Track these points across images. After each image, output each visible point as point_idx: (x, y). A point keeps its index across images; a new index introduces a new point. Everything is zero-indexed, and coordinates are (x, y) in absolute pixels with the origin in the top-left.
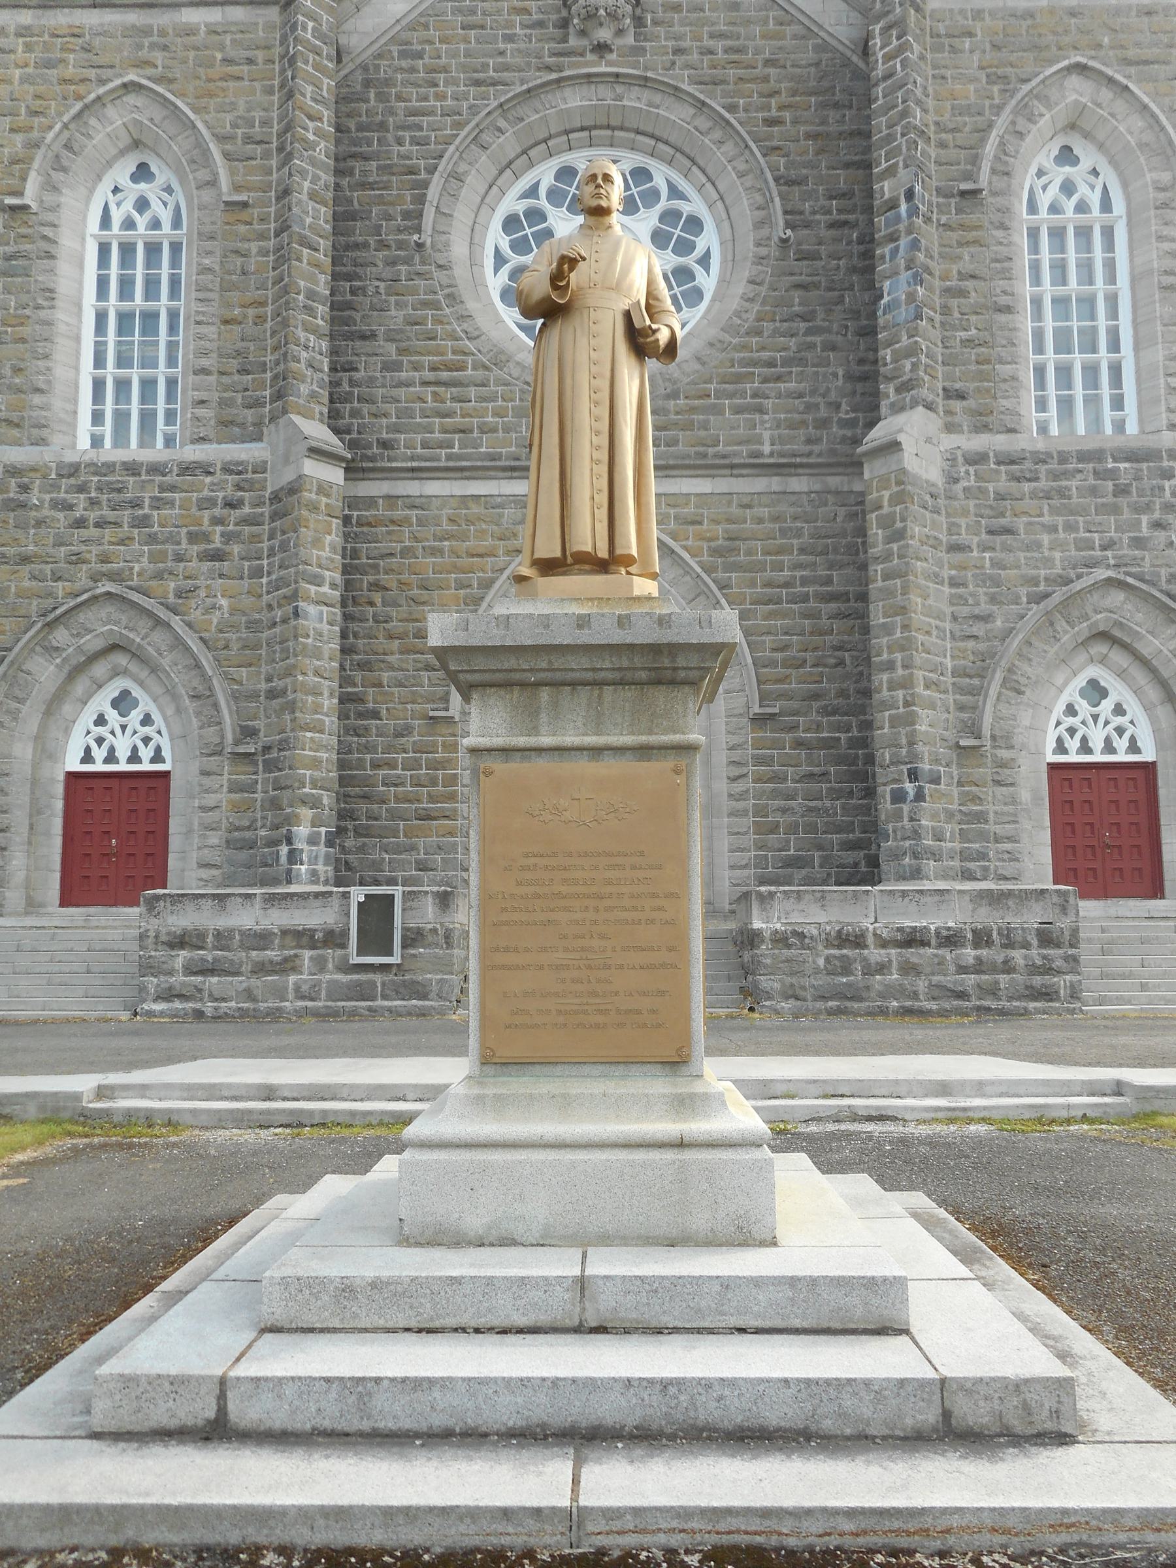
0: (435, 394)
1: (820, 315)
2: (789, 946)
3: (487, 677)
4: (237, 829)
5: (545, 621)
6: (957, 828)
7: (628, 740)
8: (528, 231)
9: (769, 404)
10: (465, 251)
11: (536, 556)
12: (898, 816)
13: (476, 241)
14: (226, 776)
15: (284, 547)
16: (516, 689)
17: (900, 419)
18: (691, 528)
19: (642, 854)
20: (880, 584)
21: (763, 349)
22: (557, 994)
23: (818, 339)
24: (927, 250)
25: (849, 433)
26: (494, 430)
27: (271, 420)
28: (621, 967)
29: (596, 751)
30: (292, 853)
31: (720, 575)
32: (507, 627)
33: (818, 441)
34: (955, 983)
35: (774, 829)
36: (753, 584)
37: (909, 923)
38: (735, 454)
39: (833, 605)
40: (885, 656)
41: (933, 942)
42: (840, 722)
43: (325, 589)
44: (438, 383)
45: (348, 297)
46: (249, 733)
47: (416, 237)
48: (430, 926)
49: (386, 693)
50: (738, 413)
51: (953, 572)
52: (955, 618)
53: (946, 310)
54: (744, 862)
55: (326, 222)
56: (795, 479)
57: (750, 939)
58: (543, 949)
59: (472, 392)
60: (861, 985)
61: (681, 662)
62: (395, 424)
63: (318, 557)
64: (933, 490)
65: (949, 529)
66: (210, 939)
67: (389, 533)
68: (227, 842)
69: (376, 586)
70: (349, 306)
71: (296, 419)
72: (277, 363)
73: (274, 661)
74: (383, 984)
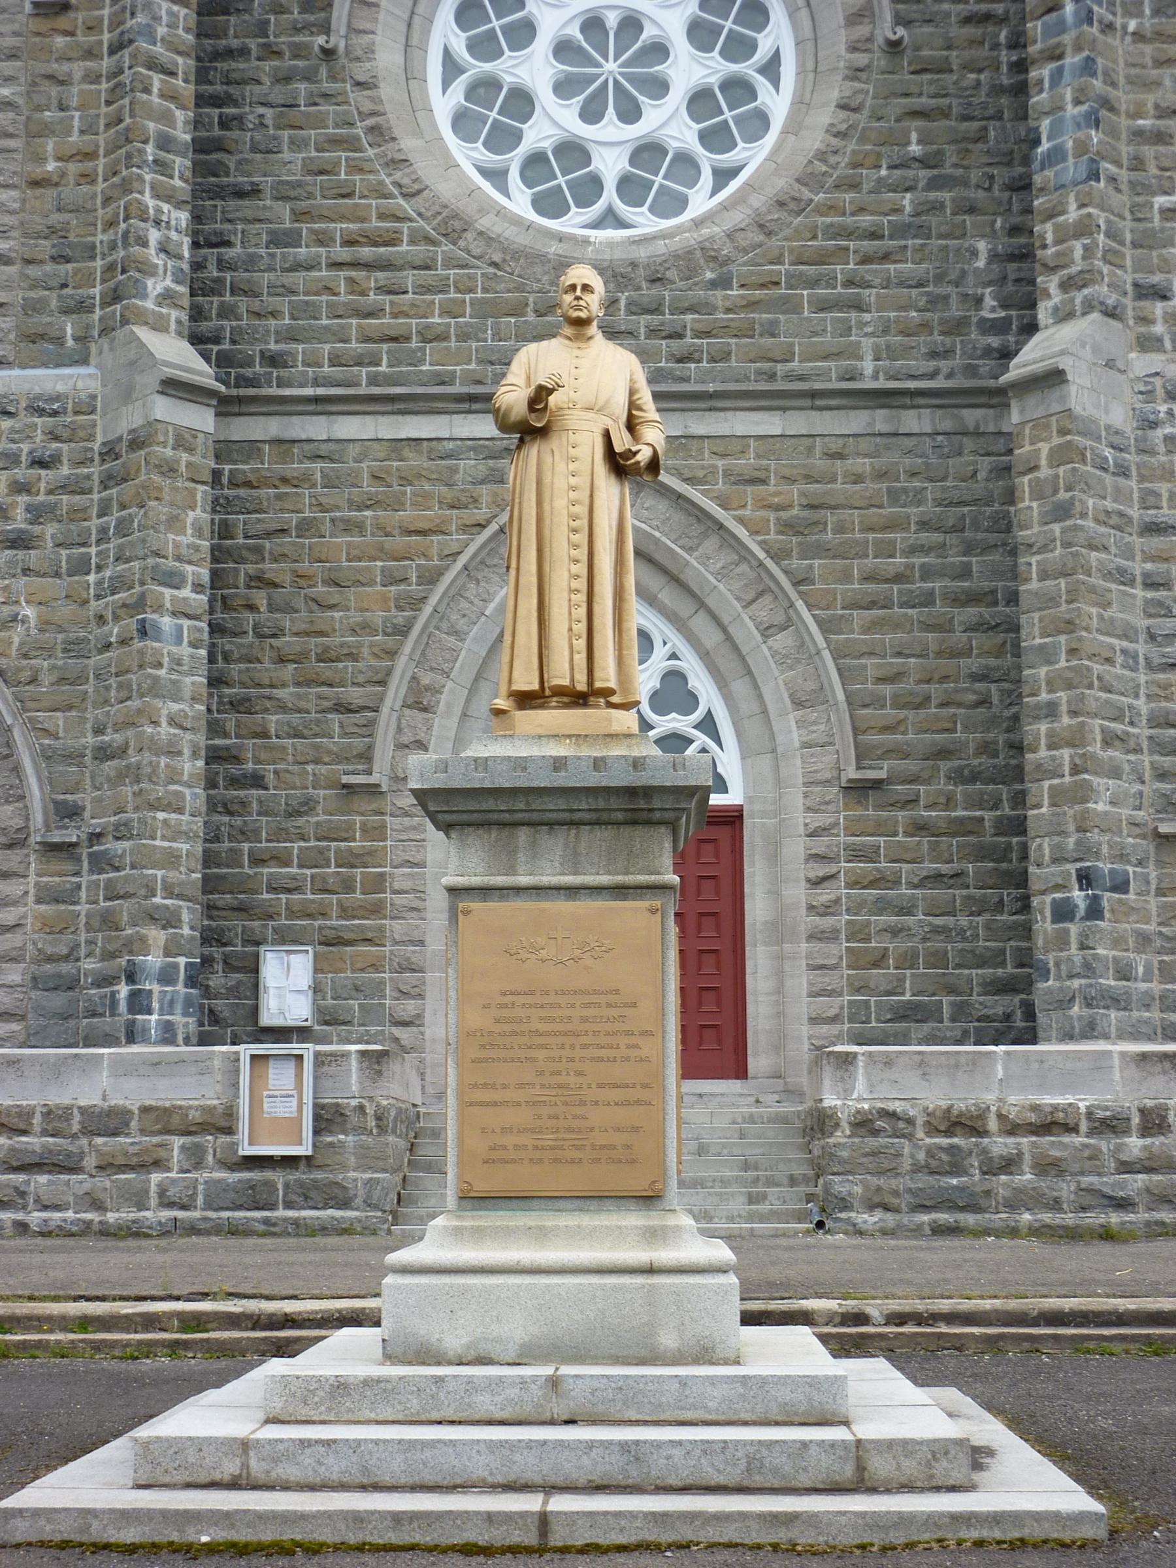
0: (351, 281)
1: (951, 158)
2: (876, 1133)
3: (465, 817)
4: (50, 959)
5: (521, 764)
6: (1156, 960)
7: (604, 879)
8: (496, 24)
9: (870, 295)
10: (399, 59)
11: (514, 688)
12: (1062, 941)
13: (414, 41)
14: (32, 879)
15: (123, 528)
16: (494, 829)
17: (1068, 332)
18: (749, 489)
19: (617, 992)
20: (1034, 585)
21: (862, 210)
22: (533, 1131)
23: (946, 196)
24: (1106, 74)
25: (994, 341)
26: (443, 337)
27: (104, 332)
28: (597, 1103)
29: (572, 891)
30: (134, 995)
31: (795, 563)
32: (486, 770)
33: (947, 353)
34: (1113, 1185)
35: (879, 961)
36: (847, 577)
37: (1049, 1100)
38: (822, 375)
39: (972, 611)
40: (1044, 696)
41: (1084, 1126)
42: (982, 793)
43: (186, 592)
44: (355, 265)
45: (217, 132)
46: (68, 812)
47: (321, 40)
48: (354, 1102)
49: (272, 748)
50: (822, 310)
51: (1149, 566)
52: (1152, 637)
53: (1138, 164)
54: (832, 1012)
55: (187, 30)
56: (912, 412)
57: (820, 1122)
58: (521, 1086)
59: (410, 278)
60: (978, 1189)
61: (656, 804)
62: (290, 328)
63: (177, 545)
64: (1117, 440)
65: (1143, 500)
66: (37, 1120)
67: (279, 497)
68: (34, 979)
69: (259, 581)
70: (219, 146)
71: (143, 333)
72: (113, 246)
73: (106, 702)
74: (287, 1186)
